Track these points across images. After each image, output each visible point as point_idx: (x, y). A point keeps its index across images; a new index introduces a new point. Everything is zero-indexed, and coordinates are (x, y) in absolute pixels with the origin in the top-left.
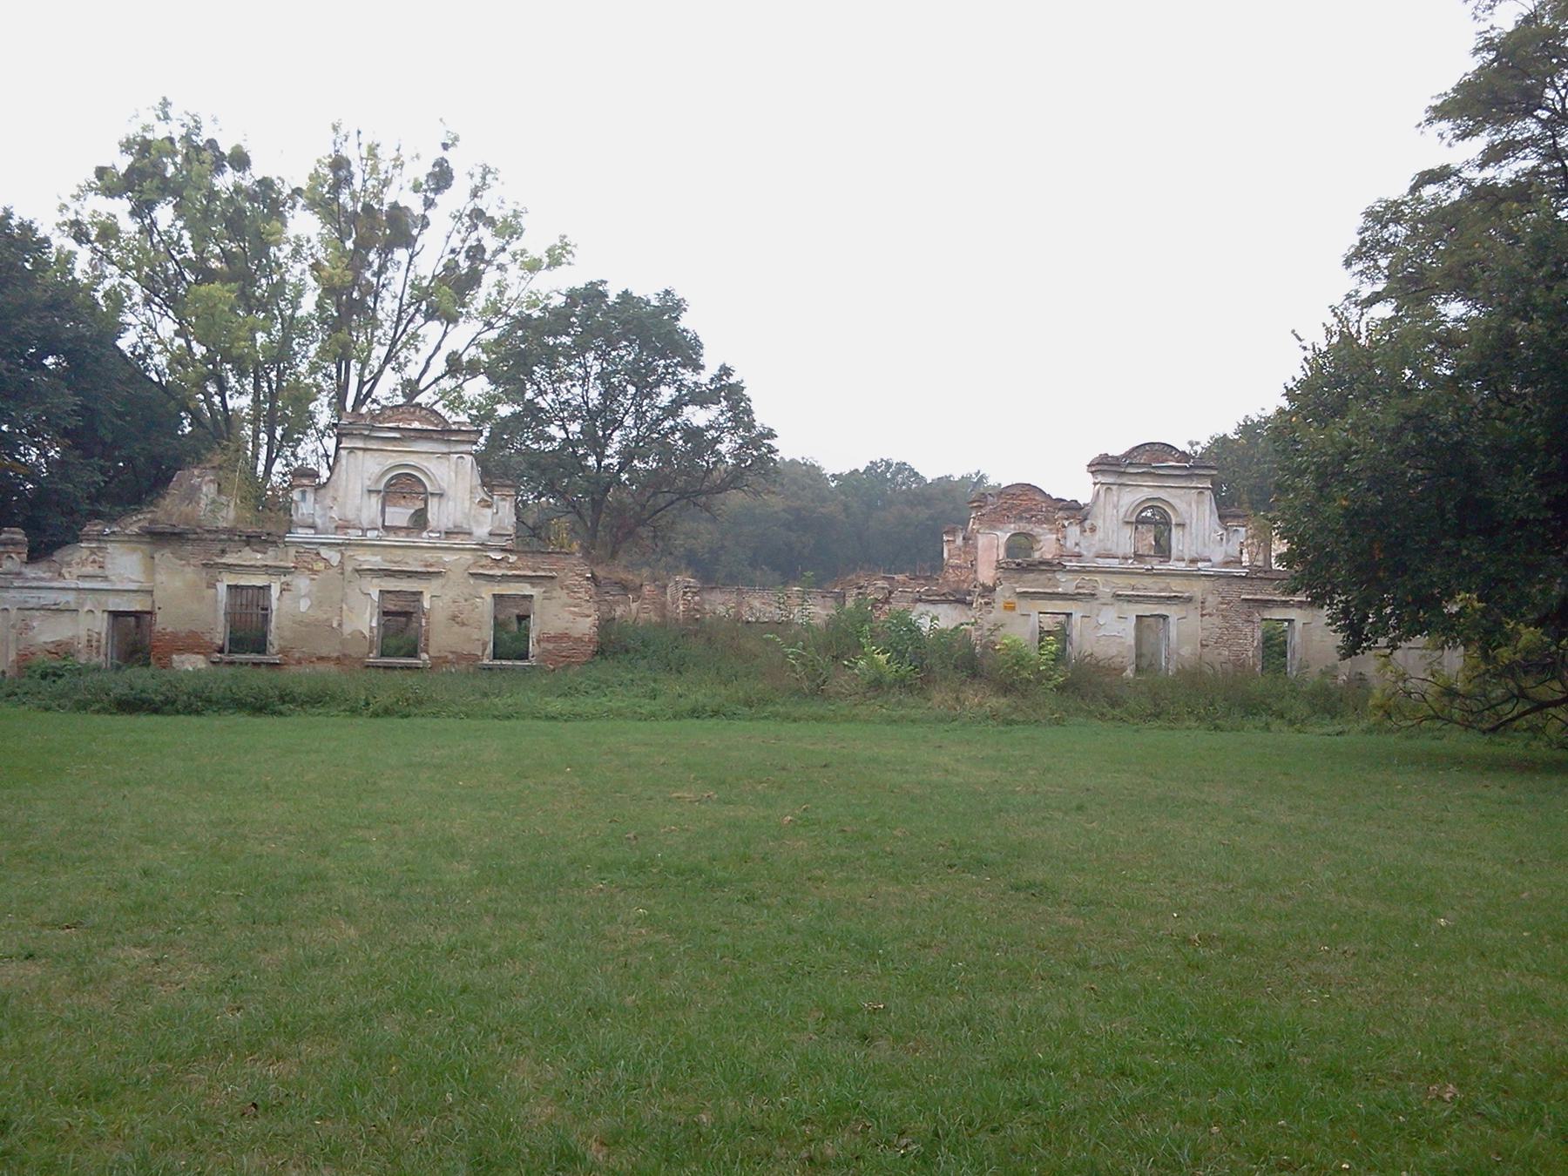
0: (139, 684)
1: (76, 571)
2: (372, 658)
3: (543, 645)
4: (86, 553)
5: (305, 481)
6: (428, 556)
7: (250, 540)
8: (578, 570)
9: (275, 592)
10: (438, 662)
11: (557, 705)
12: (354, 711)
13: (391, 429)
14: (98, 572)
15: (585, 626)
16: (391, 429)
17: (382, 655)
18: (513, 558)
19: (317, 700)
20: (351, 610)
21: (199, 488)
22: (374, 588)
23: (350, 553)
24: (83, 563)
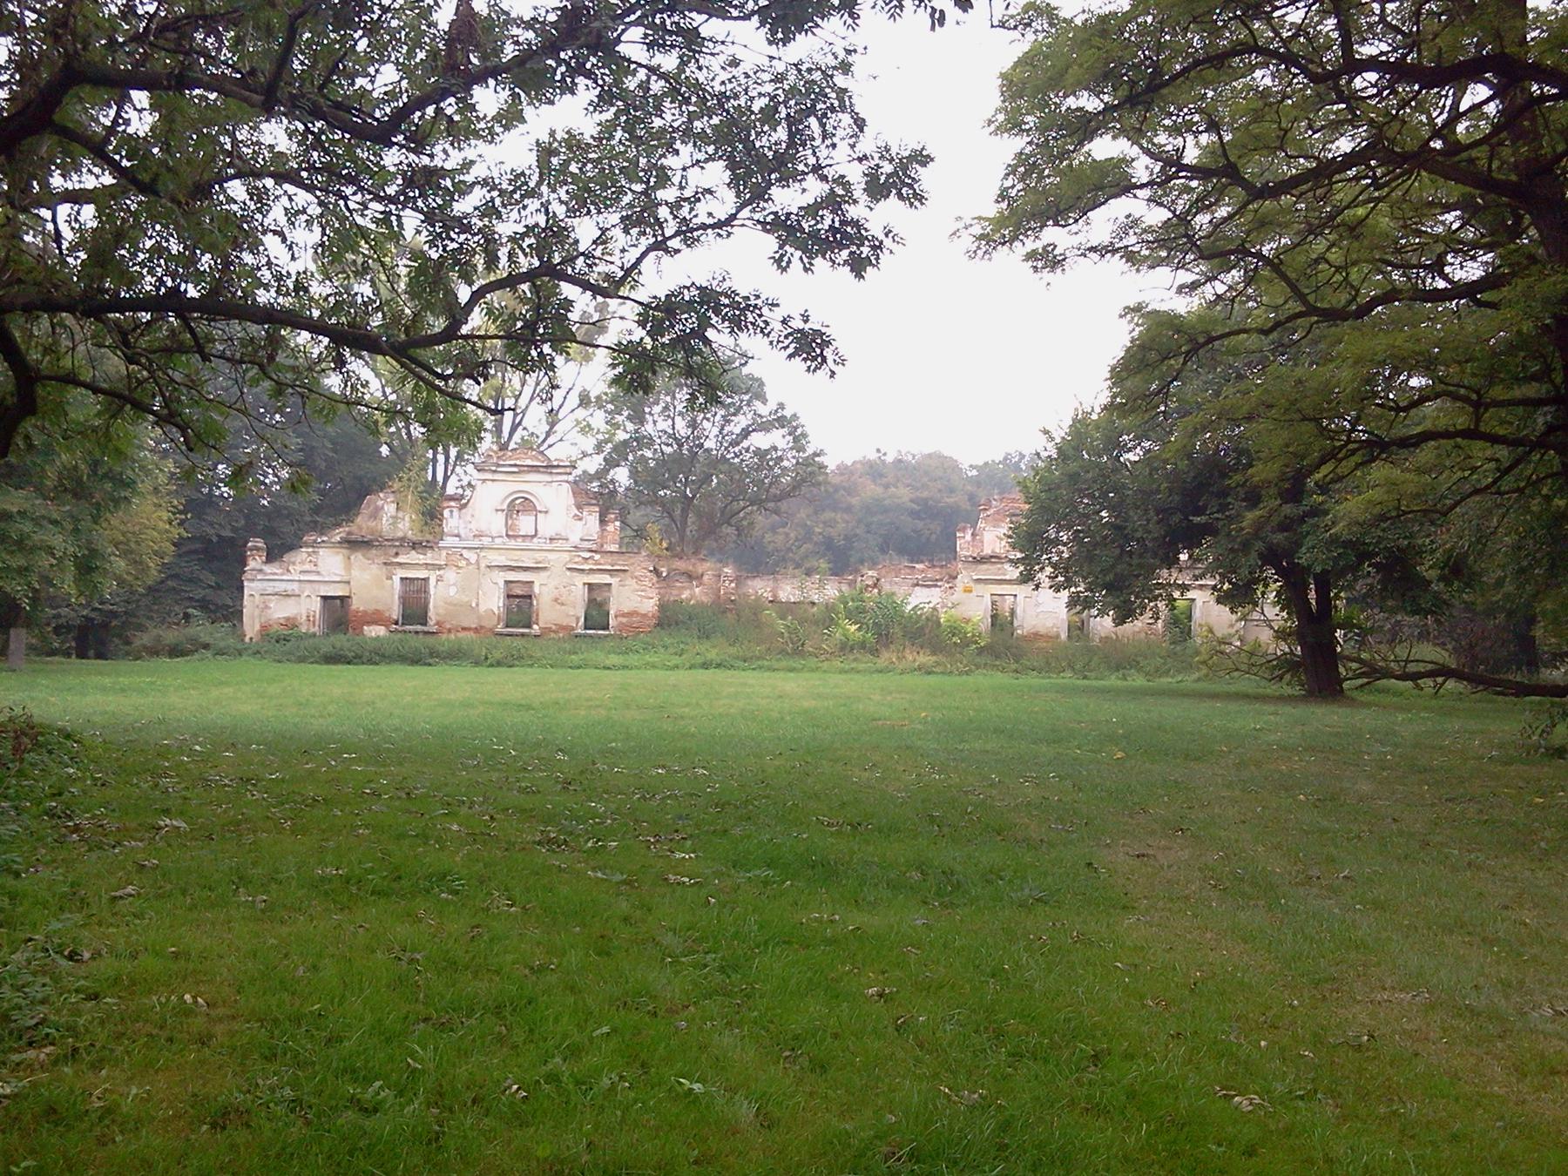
0: (338, 645)
1: (299, 568)
2: (500, 629)
3: (620, 619)
4: (305, 555)
5: (452, 504)
6: (539, 555)
7: (415, 546)
8: (643, 565)
9: (432, 582)
10: (546, 631)
11: (614, 659)
12: (477, 663)
13: (511, 466)
14: (314, 568)
15: (649, 605)
16: (511, 466)
17: (507, 627)
18: (597, 557)
19: (455, 656)
20: (484, 594)
21: (383, 508)
22: (501, 577)
23: (482, 554)
24: (302, 563)
